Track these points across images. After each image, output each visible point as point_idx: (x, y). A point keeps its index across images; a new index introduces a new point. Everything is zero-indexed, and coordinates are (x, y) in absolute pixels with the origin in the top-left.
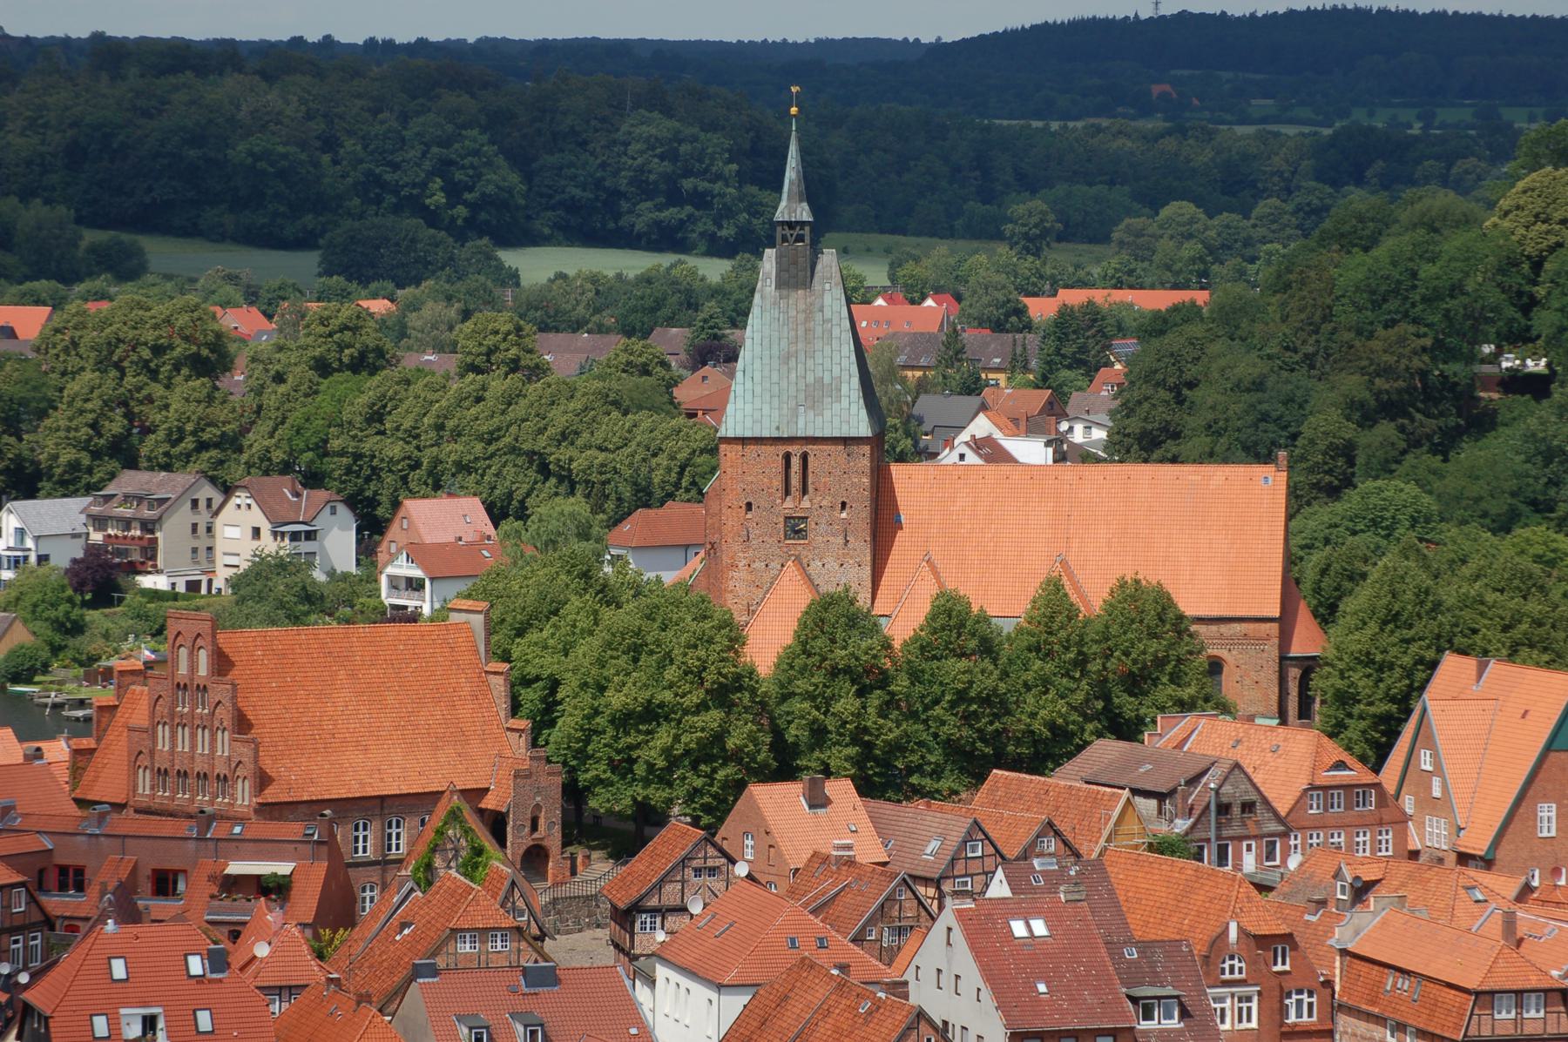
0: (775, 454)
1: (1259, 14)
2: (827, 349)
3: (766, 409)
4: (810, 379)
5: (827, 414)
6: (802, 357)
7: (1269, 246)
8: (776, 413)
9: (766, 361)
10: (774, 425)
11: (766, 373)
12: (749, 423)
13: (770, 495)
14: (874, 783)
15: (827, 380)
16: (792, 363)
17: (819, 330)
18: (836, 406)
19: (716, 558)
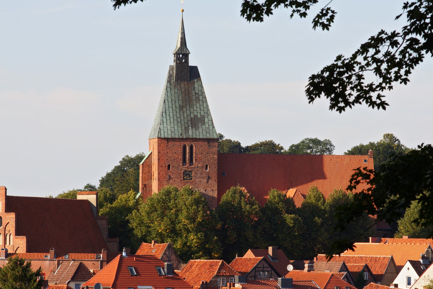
0: (178, 146)
1: (123, 4)
2: (198, 105)
3: (176, 127)
4: (192, 116)
5: (200, 130)
6: (188, 108)
7: (242, 205)
8: (180, 129)
9: (174, 108)
10: (180, 134)
11: (175, 113)
12: (169, 132)
13: (177, 162)
14: (390, 149)
15: (199, 116)
16: (185, 109)
17: (194, 97)
18: (204, 127)
19: (146, 190)
